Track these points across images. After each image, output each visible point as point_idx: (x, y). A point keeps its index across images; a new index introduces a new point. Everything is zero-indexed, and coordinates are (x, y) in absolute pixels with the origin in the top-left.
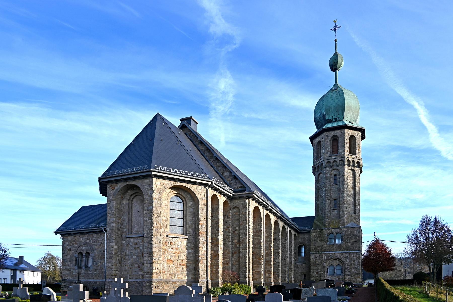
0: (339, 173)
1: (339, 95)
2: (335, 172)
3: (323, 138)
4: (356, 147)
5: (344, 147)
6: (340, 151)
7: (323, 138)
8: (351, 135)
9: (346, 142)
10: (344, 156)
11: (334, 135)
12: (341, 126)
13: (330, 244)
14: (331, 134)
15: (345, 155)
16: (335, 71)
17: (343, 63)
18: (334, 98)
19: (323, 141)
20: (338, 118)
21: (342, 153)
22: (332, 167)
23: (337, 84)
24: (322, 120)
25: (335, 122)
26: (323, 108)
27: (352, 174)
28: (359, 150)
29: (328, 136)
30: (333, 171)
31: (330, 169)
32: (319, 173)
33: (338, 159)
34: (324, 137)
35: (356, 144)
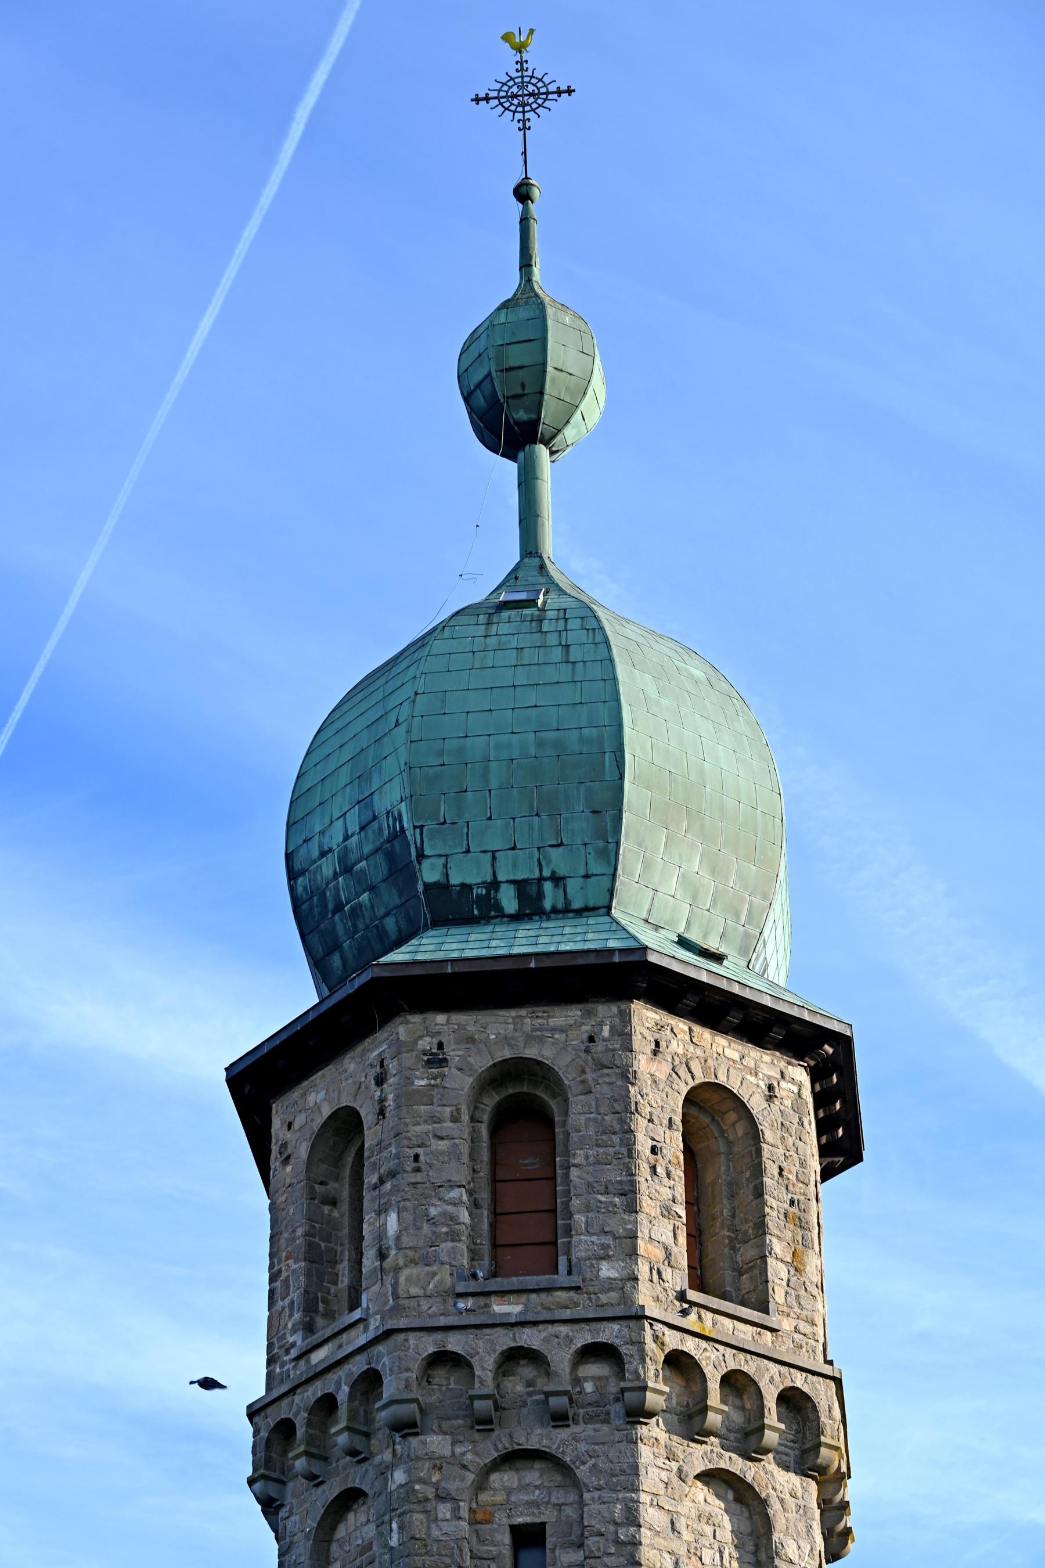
0: (569, 1511)
1: (557, 654)
2: (524, 1488)
3: (380, 1081)
4: (761, 1227)
5: (632, 1208)
6: (583, 1244)
7: (380, 1081)
8: (700, 1079)
9: (643, 1145)
10: (626, 1299)
11: (507, 1054)
12: (592, 960)
13: (437, 1278)
14: (471, 1040)
15: (646, 1297)
16: (521, 447)
17: (598, 384)
18: (507, 677)
19: (382, 1113)
20: (548, 886)
21: (607, 1271)
22: (484, 1424)
23: (542, 567)
24: (372, 889)
25: (517, 918)
26: (391, 766)
27: (726, 1533)
28: (796, 1265)
29: (436, 1060)
30: (495, 1478)
31: (466, 1452)
32: (332, 1489)
33: (564, 1329)
34: (392, 1067)
35: (759, 1192)
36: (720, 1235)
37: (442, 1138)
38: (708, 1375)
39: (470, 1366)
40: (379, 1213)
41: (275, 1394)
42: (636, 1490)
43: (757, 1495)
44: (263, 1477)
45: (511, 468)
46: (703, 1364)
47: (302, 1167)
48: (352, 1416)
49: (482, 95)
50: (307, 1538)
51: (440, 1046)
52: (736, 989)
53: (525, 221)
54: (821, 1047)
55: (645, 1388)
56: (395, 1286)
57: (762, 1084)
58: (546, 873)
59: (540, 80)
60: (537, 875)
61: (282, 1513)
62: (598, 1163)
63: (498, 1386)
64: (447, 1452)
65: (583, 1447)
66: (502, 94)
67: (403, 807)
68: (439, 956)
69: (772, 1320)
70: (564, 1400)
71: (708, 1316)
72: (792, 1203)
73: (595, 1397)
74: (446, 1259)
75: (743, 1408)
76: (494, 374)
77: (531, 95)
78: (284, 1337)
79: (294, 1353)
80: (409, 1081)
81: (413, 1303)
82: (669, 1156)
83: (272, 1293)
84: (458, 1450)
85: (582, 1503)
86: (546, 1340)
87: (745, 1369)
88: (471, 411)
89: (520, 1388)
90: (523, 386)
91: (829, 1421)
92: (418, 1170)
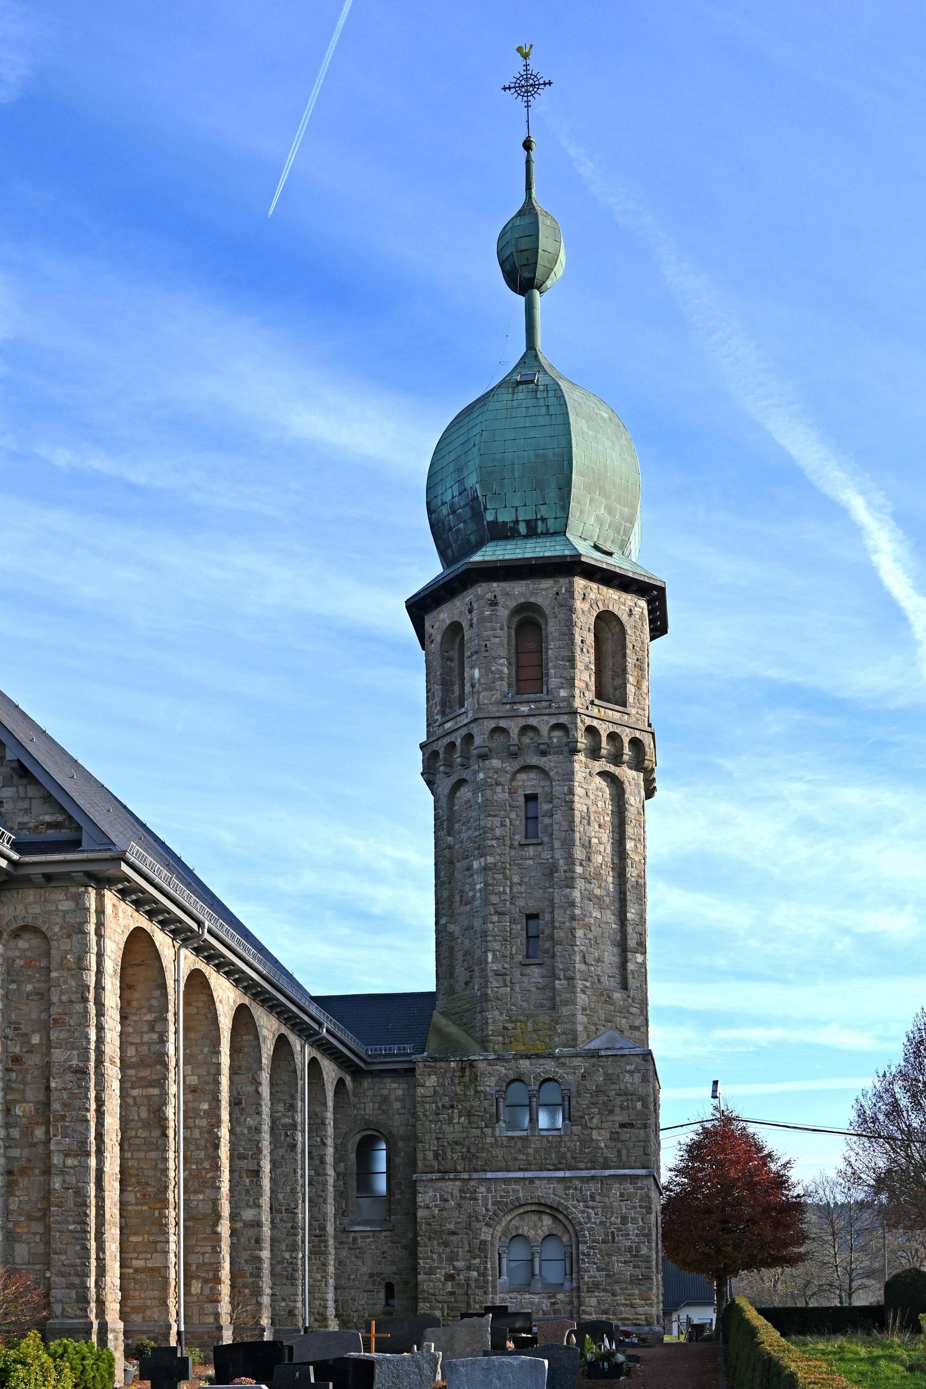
1: (543, 410)
2: (529, 780)
3: (470, 611)
5: (573, 667)
6: (554, 682)
7: (470, 611)
8: (602, 609)
10: (570, 706)
12: (558, 560)
14: (508, 594)
15: (578, 703)
17: (562, 257)
19: (471, 625)
20: (539, 523)
22: (514, 755)
23: (536, 356)
24: (465, 522)
25: (527, 537)
26: (472, 466)
27: (607, 795)
28: (638, 686)
30: (519, 776)
32: (454, 779)
33: (545, 718)
34: (475, 605)
35: (624, 656)
36: (608, 674)
37: (496, 637)
38: (602, 735)
39: (508, 732)
40: (471, 668)
41: (431, 740)
42: (573, 781)
43: (620, 780)
44: (427, 773)
45: (521, 300)
46: (600, 730)
47: (438, 645)
48: (462, 751)
49: (507, 86)
50: (445, 796)
51: (495, 597)
52: (617, 570)
53: (528, 162)
54: (652, 592)
55: (577, 741)
56: (478, 700)
57: (627, 609)
58: (539, 517)
59: (535, 77)
60: (535, 518)
61: (435, 786)
62: (560, 648)
63: (519, 740)
64: (500, 766)
65: (552, 764)
66: (517, 85)
67: (477, 486)
68: (494, 558)
69: (628, 710)
70: (545, 746)
71: (602, 710)
72: (638, 660)
73: (557, 745)
74: (498, 688)
75: (615, 746)
76: (514, 254)
77: (531, 85)
78: (433, 716)
79: (438, 723)
80: (482, 613)
81: (486, 707)
82: (588, 644)
83: (427, 697)
84: (504, 765)
85: (552, 786)
86: (538, 722)
87: (616, 731)
88: (503, 271)
89: (528, 741)
90: (528, 260)
91: (649, 750)
92: (487, 651)
